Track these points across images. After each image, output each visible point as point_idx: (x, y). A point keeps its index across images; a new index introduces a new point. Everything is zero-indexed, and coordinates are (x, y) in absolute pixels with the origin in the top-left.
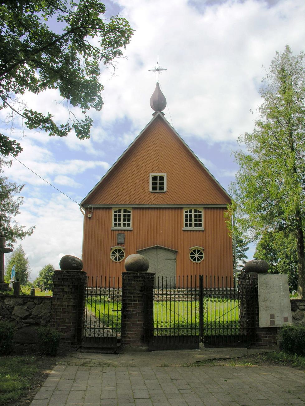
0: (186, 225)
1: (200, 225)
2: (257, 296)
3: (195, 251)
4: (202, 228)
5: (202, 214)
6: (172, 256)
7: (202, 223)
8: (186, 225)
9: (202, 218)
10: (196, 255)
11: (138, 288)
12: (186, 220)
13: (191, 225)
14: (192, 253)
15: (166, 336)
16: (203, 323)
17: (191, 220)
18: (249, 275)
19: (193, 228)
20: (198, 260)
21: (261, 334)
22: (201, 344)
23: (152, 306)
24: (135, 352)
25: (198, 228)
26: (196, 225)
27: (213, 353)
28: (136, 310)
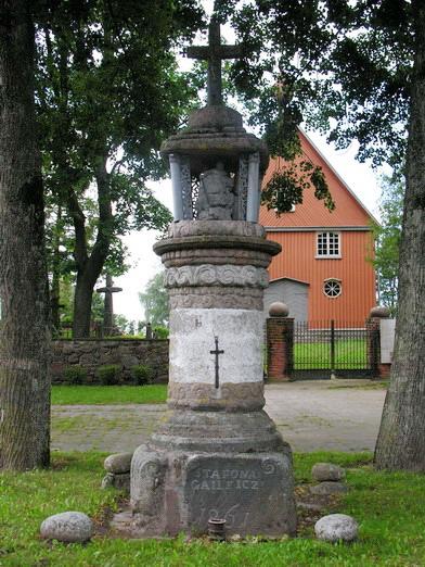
0: (320, 253)
1: (337, 252)
2: (379, 337)
3: (330, 284)
4: (339, 256)
5: (339, 238)
6: (302, 289)
7: (339, 249)
8: (320, 253)
9: (339, 243)
10: (332, 286)
11: (281, 331)
12: (320, 246)
13: (325, 252)
14: (327, 287)
15: (228, 459)
16: (89, 312)
17: (325, 246)
18: (374, 320)
19: (328, 256)
20: (335, 294)
21: (380, 367)
22: (333, 376)
23: (292, 345)
24: (278, 382)
25: (334, 256)
26: (331, 252)
27: (342, 381)
28: (279, 349)
